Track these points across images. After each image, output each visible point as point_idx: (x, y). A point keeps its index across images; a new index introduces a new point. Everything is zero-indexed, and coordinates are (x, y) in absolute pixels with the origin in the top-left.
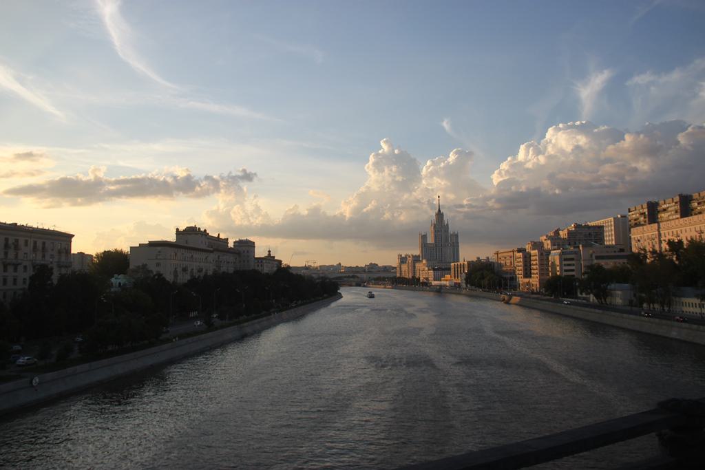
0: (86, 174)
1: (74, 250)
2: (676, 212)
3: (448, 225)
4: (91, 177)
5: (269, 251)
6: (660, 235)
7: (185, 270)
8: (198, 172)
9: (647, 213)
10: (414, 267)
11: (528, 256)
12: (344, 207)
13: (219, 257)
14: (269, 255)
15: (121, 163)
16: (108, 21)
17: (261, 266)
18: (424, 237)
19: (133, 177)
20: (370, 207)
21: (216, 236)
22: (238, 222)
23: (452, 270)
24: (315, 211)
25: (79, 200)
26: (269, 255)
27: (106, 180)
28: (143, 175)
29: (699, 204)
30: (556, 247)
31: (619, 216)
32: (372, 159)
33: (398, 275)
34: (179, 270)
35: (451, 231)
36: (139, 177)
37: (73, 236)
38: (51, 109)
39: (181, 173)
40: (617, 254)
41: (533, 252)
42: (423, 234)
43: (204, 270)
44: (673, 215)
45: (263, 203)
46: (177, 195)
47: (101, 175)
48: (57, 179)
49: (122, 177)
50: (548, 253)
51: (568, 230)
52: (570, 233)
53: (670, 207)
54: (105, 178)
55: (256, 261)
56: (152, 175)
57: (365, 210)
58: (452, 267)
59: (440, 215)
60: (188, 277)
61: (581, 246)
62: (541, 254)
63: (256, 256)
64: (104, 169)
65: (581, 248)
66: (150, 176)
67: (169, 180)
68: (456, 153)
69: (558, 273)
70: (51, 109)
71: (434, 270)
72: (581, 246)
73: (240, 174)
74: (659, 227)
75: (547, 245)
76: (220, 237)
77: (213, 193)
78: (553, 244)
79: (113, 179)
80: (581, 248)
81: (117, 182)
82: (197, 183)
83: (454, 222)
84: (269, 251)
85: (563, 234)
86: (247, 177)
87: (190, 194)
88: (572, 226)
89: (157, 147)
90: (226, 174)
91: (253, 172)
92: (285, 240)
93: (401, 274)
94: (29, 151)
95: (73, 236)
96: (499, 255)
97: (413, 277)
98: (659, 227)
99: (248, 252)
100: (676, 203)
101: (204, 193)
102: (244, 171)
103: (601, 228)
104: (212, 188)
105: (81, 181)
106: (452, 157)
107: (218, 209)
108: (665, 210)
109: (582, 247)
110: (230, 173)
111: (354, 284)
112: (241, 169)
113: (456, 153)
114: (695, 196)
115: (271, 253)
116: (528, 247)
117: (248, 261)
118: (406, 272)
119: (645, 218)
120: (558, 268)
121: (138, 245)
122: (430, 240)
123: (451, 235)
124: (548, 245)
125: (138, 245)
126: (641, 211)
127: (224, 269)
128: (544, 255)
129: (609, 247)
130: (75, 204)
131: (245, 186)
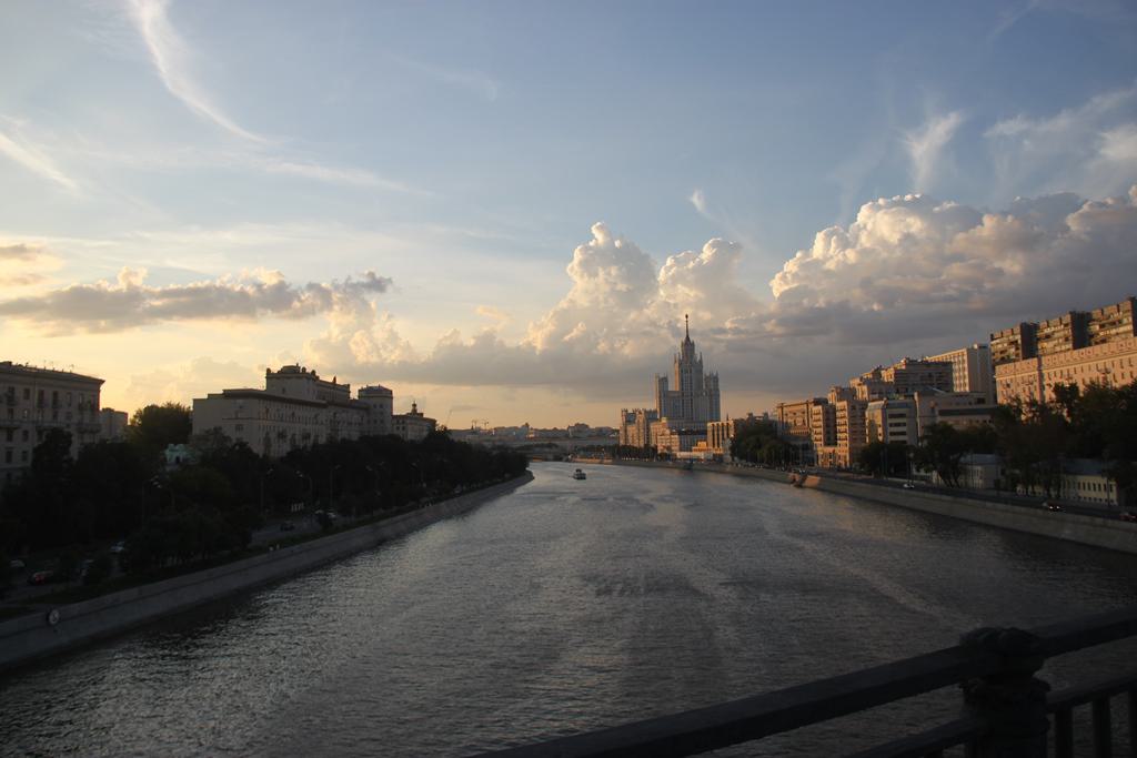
0: (114, 280)
1: (103, 405)
2: (1067, 339)
3: (701, 361)
4: (122, 286)
5: (414, 405)
6: (1041, 376)
7: (281, 436)
8: (297, 278)
9: (1020, 342)
10: (648, 429)
11: (831, 411)
12: (533, 333)
13: (335, 414)
14: (415, 411)
15: (170, 263)
16: (147, 30)
17: (404, 428)
18: (663, 381)
19: (191, 285)
20: (575, 333)
21: (331, 380)
22: (361, 359)
23: (710, 434)
24: (486, 340)
25: (103, 323)
26: (415, 411)
27: (146, 291)
28: (207, 282)
29: (1102, 326)
30: (876, 396)
31: (976, 347)
32: (578, 255)
33: (622, 442)
34: (273, 436)
35: (706, 370)
36: (200, 285)
37: (103, 382)
38: (54, 174)
39: (269, 279)
40: (975, 407)
41: (839, 405)
42: (662, 376)
43: (312, 438)
44: (1059, 344)
45: (401, 326)
46: (263, 314)
47: (138, 282)
48: (67, 288)
49: (172, 286)
50: (864, 405)
51: (896, 369)
52: (898, 373)
53: (1057, 331)
54: (144, 287)
55: (395, 421)
56: (222, 282)
57: (567, 338)
58: (710, 429)
59: (688, 345)
60: (286, 448)
61: (916, 394)
62: (852, 408)
63: (395, 413)
64: (143, 272)
65: (916, 398)
66: (218, 283)
67: (250, 290)
68: (713, 246)
69: (880, 438)
70: (54, 174)
71: (680, 433)
72: (916, 394)
73: (365, 280)
74: (1040, 365)
75: (863, 393)
76: (337, 382)
77: (321, 310)
78: (872, 392)
79: (159, 289)
80: (916, 398)
81: (165, 294)
82: (295, 295)
83: (712, 356)
84: (414, 405)
85: (888, 376)
86: (377, 285)
87: (285, 313)
88: (901, 365)
89: (229, 237)
90: (341, 281)
91: (387, 277)
92: (437, 387)
93: (626, 440)
94: (18, 244)
95: (103, 382)
96: (785, 409)
97: (647, 446)
98: (1040, 365)
99: (381, 406)
100: (1066, 325)
101: (307, 312)
102: (371, 275)
103: (947, 365)
104: (319, 302)
105: (106, 291)
106: (707, 253)
107: (329, 338)
108: (1048, 337)
109: (919, 395)
110: (349, 278)
111: (551, 457)
112: (366, 272)
113: (713, 246)
114: (1096, 314)
115: (418, 407)
116: (831, 397)
117: (382, 421)
118: (635, 438)
119: (1017, 349)
120: (880, 430)
121: (206, 397)
122: (674, 386)
123: (707, 378)
124: (863, 392)
125: (206, 397)
126: (1011, 337)
127: (343, 434)
128: (858, 409)
129: (960, 395)
130: (96, 330)
131: (373, 300)
